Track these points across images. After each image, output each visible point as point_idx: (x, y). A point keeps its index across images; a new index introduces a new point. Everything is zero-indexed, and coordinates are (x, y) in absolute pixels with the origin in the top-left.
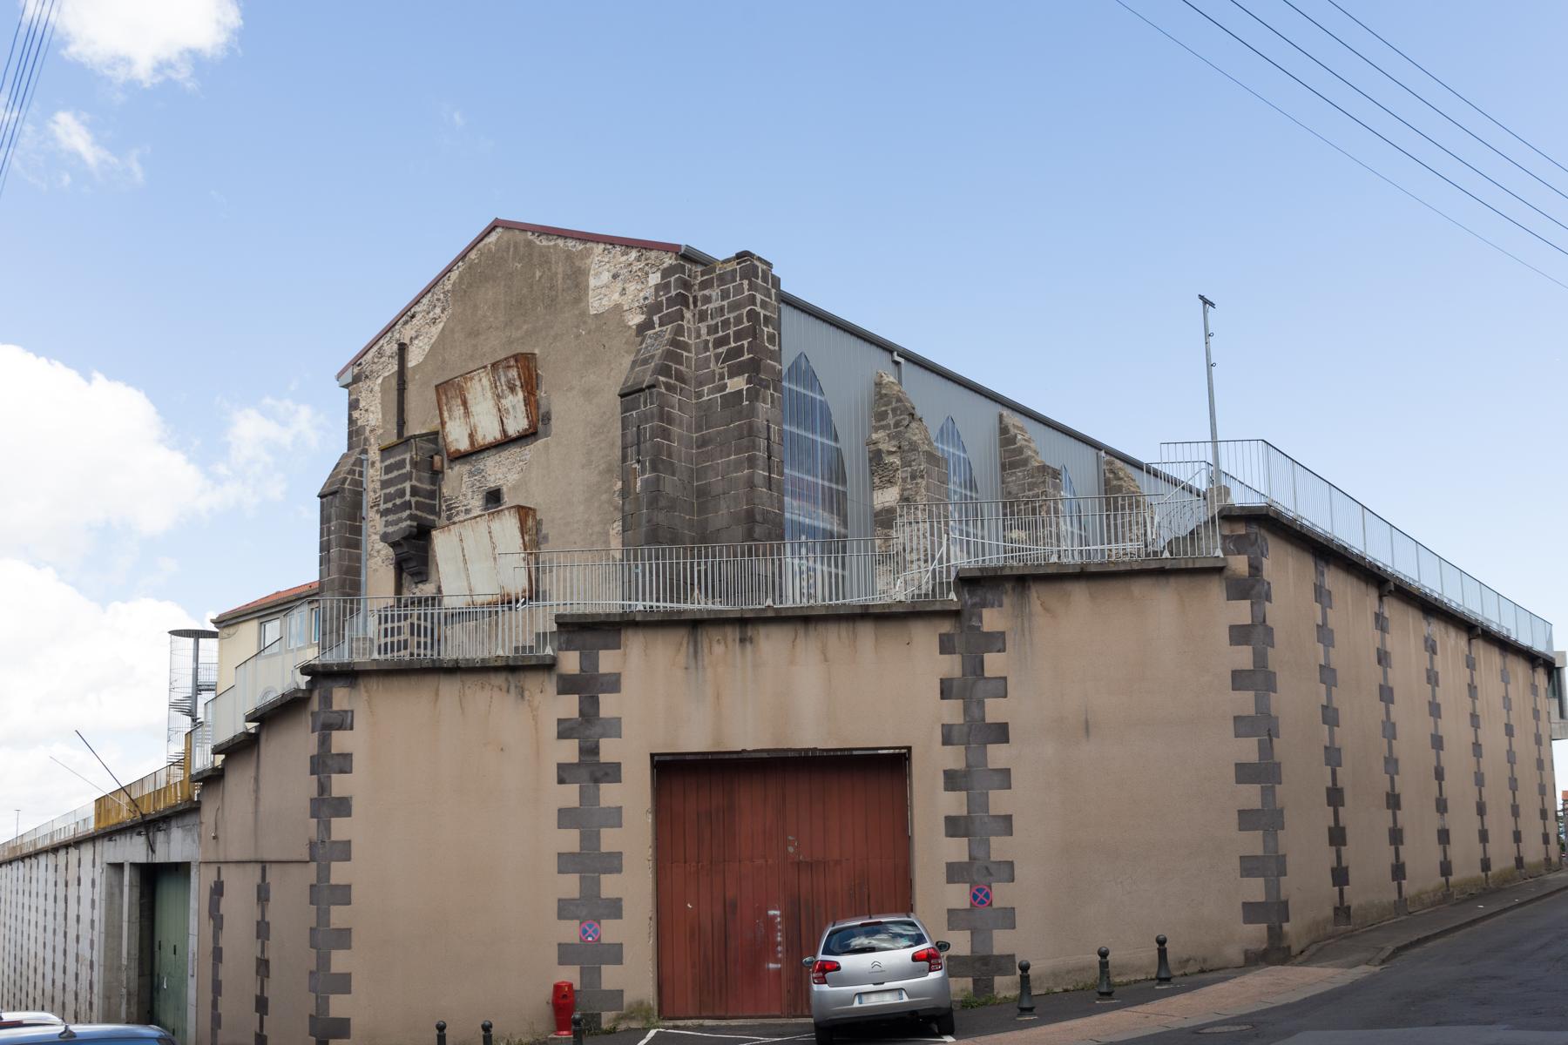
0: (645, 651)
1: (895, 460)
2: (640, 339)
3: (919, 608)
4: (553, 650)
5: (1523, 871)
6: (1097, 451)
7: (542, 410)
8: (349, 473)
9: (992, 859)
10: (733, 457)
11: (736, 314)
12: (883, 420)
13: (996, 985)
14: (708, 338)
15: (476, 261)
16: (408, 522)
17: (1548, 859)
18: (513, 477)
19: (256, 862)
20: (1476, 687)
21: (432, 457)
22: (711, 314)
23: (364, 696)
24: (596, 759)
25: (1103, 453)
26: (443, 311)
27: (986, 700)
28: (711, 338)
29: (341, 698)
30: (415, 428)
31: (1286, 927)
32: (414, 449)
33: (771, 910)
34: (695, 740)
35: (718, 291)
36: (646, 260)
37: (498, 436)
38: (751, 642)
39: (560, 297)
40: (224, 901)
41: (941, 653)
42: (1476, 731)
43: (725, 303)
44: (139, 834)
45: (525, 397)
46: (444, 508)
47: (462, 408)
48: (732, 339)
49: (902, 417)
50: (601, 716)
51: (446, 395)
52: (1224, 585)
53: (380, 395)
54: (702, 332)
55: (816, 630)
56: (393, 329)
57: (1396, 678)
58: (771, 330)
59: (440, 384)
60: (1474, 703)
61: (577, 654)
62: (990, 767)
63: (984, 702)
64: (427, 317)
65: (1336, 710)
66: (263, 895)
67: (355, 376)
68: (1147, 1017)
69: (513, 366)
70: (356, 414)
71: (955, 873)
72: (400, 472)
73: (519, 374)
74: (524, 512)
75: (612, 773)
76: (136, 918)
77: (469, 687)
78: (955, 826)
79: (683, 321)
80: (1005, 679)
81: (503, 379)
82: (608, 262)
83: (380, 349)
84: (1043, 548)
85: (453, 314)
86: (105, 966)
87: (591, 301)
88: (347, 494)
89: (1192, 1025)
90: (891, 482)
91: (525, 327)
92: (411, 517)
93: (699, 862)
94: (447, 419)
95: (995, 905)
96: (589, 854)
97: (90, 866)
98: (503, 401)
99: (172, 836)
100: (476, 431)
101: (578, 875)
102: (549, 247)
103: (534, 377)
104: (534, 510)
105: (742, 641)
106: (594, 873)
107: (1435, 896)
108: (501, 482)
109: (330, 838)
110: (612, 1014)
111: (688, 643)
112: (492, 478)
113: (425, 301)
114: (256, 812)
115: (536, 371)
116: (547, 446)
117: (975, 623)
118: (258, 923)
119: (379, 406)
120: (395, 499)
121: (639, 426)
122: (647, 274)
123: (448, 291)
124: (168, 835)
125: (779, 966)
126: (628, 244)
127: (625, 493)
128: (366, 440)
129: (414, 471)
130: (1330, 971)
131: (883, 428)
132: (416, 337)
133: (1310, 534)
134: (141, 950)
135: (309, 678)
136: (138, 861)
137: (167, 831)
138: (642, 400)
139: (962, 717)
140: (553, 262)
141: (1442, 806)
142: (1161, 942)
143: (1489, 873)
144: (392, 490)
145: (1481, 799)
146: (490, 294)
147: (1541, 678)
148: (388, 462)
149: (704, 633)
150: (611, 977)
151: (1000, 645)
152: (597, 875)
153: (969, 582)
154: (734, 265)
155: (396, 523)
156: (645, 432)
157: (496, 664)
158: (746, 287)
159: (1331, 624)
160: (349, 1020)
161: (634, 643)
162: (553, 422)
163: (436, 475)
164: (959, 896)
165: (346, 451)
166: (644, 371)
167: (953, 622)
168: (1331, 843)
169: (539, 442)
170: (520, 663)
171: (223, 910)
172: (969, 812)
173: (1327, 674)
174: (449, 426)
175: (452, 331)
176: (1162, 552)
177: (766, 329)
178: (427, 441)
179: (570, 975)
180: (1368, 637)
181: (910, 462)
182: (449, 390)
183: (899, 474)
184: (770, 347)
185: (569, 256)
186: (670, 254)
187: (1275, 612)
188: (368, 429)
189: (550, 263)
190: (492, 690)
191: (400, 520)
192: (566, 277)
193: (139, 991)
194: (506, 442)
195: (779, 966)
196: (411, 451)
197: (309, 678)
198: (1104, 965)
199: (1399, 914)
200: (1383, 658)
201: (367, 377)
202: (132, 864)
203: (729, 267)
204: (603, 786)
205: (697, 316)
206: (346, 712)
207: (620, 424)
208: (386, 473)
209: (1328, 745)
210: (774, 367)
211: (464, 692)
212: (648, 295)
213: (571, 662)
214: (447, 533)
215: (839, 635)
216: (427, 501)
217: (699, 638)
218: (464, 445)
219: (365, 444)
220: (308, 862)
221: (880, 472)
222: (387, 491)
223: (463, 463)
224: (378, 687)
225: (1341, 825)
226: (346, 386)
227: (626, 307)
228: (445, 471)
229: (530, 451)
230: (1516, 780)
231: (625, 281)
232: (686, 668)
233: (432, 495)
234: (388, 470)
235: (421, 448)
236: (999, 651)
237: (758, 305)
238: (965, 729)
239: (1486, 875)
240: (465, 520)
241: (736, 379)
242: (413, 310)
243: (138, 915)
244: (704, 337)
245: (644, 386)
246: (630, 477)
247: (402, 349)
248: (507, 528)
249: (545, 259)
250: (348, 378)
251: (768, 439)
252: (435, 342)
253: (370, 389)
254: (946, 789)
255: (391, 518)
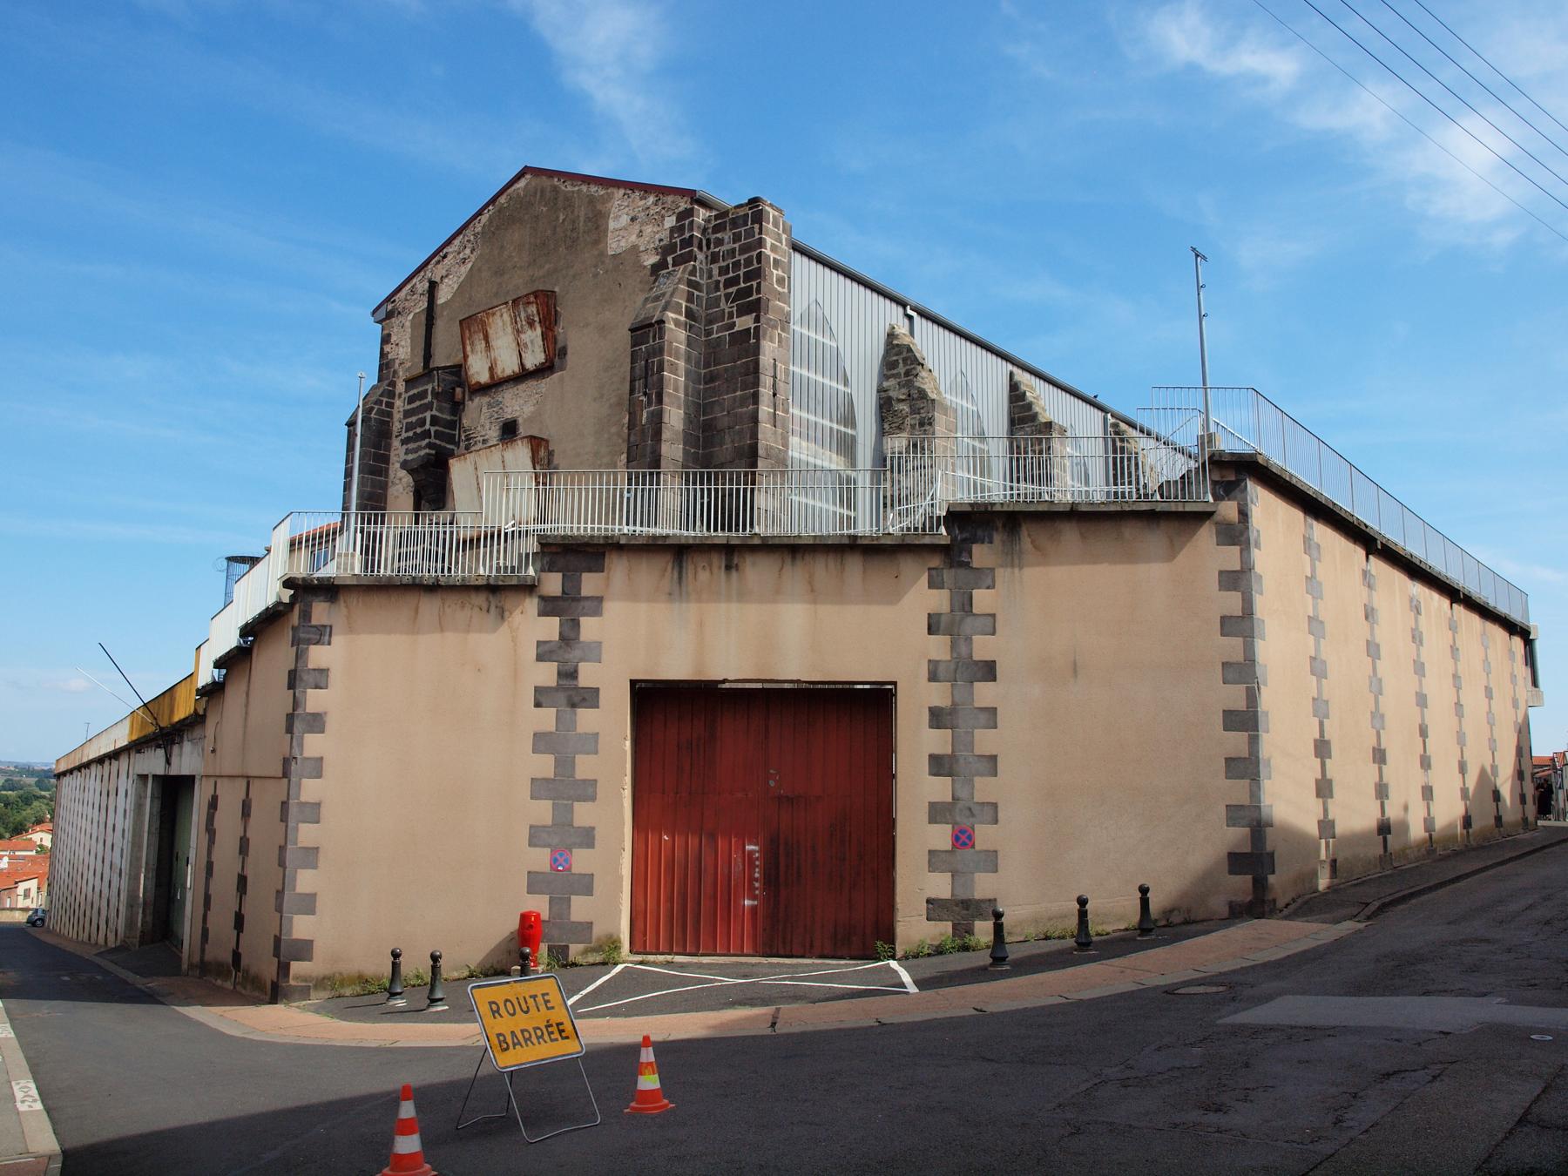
0: (629, 575)
1: (905, 407)
2: (653, 278)
3: (908, 541)
4: (536, 571)
5: (1502, 829)
6: (1103, 414)
7: (559, 345)
8: (376, 403)
9: (975, 800)
10: (738, 393)
11: (746, 256)
12: (894, 369)
13: (976, 930)
14: (719, 278)
15: (505, 205)
16: (427, 451)
17: (1525, 820)
18: (528, 409)
19: (242, 776)
20: (1457, 649)
21: (454, 389)
22: (723, 256)
23: (344, 610)
24: (575, 683)
25: (1109, 415)
26: (473, 251)
27: (974, 637)
28: (722, 279)
29: (321, 612)
30: (441, 359)
31: (1272, 879)
32: (436, 381)
33: (1319, 856)
34: (676, 668)
35: (731, 234)
36: (663, 204)
37: (516, 369)
38: (737, 570)
39: (581, 239)
40: (218, 815)
41: (929, 587)
42: (1458, 691)
43: (737, 245)
44: (159, 746)
45: (542, 332)
46: (463, 438)
47: (483, 342)
48: (742, 280)
49: (912, 366)
50: (582, 639)
51: (470, 331)
52: (1214, 531)
53: (410, 330)
54: (714, 273)
55: (803, 559)
56: (426, 269)
57: (1382, 635)
58: (780, 273)
59: (464, 319)
60: (1456, 664)
61: (560, 575)
62: (976, 705)
63: (971, 639)
64: (457, 257)
65: (1324, 662)
66: (245, 811)
67: (387, 312)
68: (1122, 972)
69: (533, 303)
70: (387, 348)
71: (937, 813)
72: (422, 402)
73: (538, 311)
74: (536, 443)
75: (589, 698)
76: (156, 829)
77: (449, 606)
78: (939, 765)
79: (695, 261)
80: (993, 616)
81: (523, 315)
82: (628, 206)
83: (413, 287)
84: (1038, 487)
85: (481, 254)
86: (130, 875)
87: (609, 242)
88: (373, 422)
89: (1169, 982)
90: (900, 429)
91: (547, 266)
92: (429, 446)
93: (677, 793)
94: (469, 353)
95: (978, 847)
96: (563, 781)
97: (124, 777)
98: (523, 336)
99: (184, 749)
100: (496, 364)
101: (551, 801)
102: (573, 192)
103: (553, 313)
104: (547, 441)
105: (728, 568)
106: (568, 800)
107: (1419, 851)
108: (517, 414)
109: (301, 754)
110: (581, 947)
111: (673, 568)
112: (509, 410)
113: (456, 242)
114: (245, 726)
115: (555, 308)
116: (561, 380)
117: (965, 559)
118: (241, 839)
119: (409, 341)
120: (415, 428)
121: (647, 360)
122: (663, 217)
123: (478, 233)
124: (181, 748)
125: (756, 903)
126: (646, 189)
127: (631, 426)
128: (395, 372)
129: (435, 401)
130: (1315, 926)
131: (894, 376)
132: (447, 276)
133: (1299, 485)
134: (159, 860)
135: (292, 592)
136: (158, 773)
137: (181, 742)
138: (651, 335)
139: (949, 653)
140: (576, 206)
141: (1425, 763)
142: (1144, 891)
143: (1470, 830)
144: (413, 419)
145: (1462, 757)
146: (517, 235)
147: (1517, 642)
148: (411, 393)
149: (690, 559)
150: (580, 908)
151: (989, 582)
152: (570, 802)
153: (956, 517)
154: (746, 210)
155: (415, 451)
156: (653, 366)
157: (477, 583)
158: (757, 230)
159: (1320, 575)
160: (312, 941)
161: (618, 567)
162: (569, 356)
163: (457, 407)
164: (941, 837)
165: (376, 382)
166: (655, 308)
167: (943, 557)
168: (1318, 795)
169: (555, 375)
170: (501, 583)
171: (216, 825)
172: (953, 751)
173: (1315, 624)
174: (471, 360)
175: (479, 270)
176: (1152, 495)
177: (775, 272)
178: (451, 373)
179: (540, 905)
180: (1355, 593)
181: (919, 409)
182: (473, 325)
183: (909, 421)
184: (779, 289)
185: (592, 200)
186: (685, 199)
187: (1262, 559)
188: (397, 362)
189: (574, 207)
190: (472, 609)
191: (420, 448)
192: (588, 219)
193: (155, 900)
194: (523, 376)
195: (756, 903)
196: (434, 382)
197: (292, 592)
198: (1083, 914)
199: (1384, 869)
200: (1369, 614)
201: (399, 313)
202: (155, 776)
203: (741, 212)
204: (579, 711)
205: (709, 258)
206: (325, 626)
207: (629, 360)
208: (409, 403)
209: (1316, 696)
210: (782, 309)
211: (444, 611)
212: (663, 237)
213: (553, 584)
214: (463, 462)
215: (827, 566)
216: (447, 431)
217: (684, 564)
218: (484, 378)
219: (394, 377)
220: (280, 778)
221: (890, 419)
222: (409, 420)
223: (483, 395)
224: (358, 602)
225: (1328, 777)
226: (379, 322)
227: (642, 249)
228: (466, 403)
229: (545, 385)
230: (1495, 741)
231: (642, 224)
232: (670, 594)
233: (452, 425)
234: (411, 400)
235: (444, 380)
236: (988, 588)
237: (768, 248)
238: (953, 666)
239: (1468, 832)
240: (480, 450)
241: (743, 318)
242: (445, 251)
243: (158, 826)
244: (716, 276)
245: (653, 321)
246: (636, 408)
247: (433, 286)
248: (520, 454)
249: (569, 202)
250: (382, 314)
251: (775, 377)
252: (462, 282)
253: (401, 325)
254: (931, 727)
255: (411, 446)
